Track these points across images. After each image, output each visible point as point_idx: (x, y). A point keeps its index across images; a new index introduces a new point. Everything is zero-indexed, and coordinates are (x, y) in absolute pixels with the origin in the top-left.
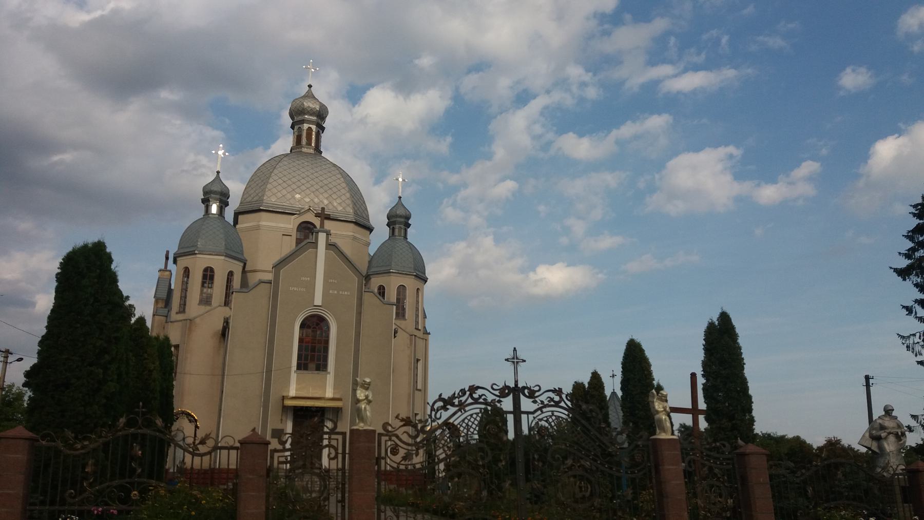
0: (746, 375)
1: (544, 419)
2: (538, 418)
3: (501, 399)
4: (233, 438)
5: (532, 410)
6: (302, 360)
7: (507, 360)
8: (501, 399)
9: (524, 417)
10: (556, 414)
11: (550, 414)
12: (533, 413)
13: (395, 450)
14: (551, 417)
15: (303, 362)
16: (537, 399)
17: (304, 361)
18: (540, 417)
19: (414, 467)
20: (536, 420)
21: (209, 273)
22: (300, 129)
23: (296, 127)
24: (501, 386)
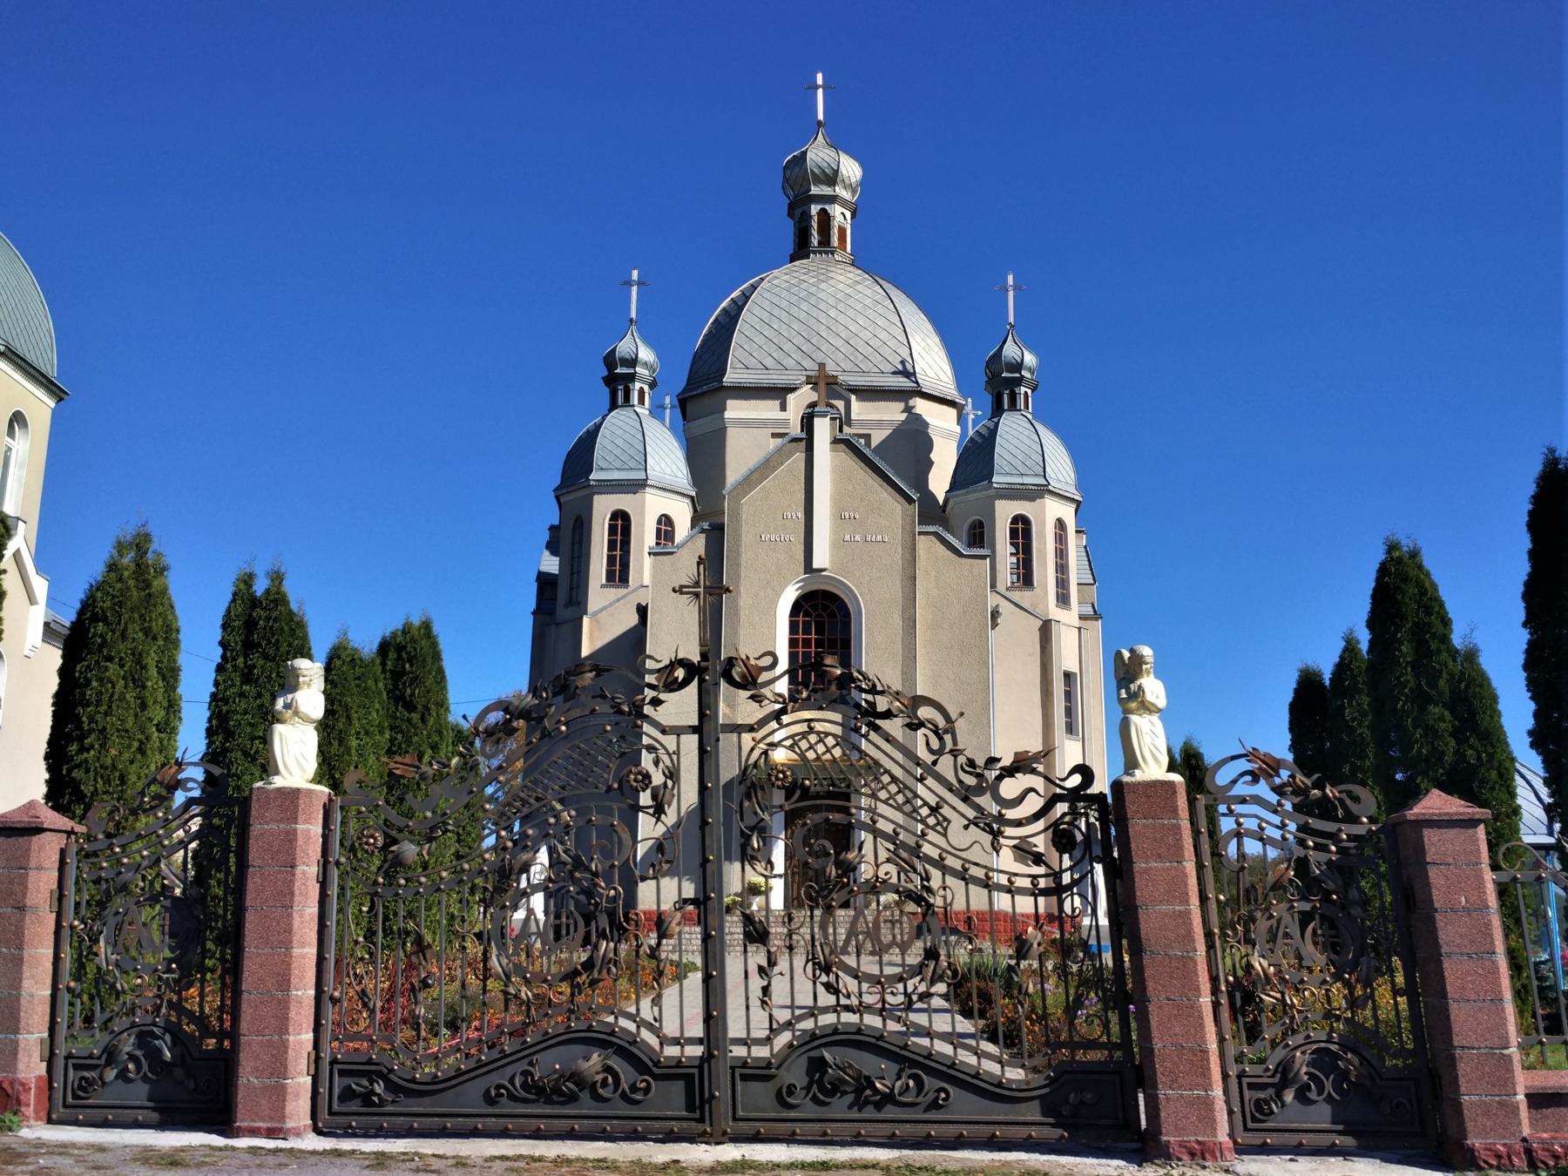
0: (1292, 695)
1: (784, 743)
2: (769, 740)
3: (662, 696)
4: (968, 849)
5: (751, 721)
6: (811, 639)
7: (679, 590)
8: (662, 696)
9: (727, 741)
10: (818, 727)
11: (803, 727)
12: (751, 729)
13: (1064, 841)
14: (804, 735)
15: (813, 636)
16: (766, 691)
17: (811, 639)
18: (777, 737)
19: (1032, 883)
20: (762, 746)
21: (1020, 526)
22: (806, 216)
23: (798, 212)
24: (666, 662)
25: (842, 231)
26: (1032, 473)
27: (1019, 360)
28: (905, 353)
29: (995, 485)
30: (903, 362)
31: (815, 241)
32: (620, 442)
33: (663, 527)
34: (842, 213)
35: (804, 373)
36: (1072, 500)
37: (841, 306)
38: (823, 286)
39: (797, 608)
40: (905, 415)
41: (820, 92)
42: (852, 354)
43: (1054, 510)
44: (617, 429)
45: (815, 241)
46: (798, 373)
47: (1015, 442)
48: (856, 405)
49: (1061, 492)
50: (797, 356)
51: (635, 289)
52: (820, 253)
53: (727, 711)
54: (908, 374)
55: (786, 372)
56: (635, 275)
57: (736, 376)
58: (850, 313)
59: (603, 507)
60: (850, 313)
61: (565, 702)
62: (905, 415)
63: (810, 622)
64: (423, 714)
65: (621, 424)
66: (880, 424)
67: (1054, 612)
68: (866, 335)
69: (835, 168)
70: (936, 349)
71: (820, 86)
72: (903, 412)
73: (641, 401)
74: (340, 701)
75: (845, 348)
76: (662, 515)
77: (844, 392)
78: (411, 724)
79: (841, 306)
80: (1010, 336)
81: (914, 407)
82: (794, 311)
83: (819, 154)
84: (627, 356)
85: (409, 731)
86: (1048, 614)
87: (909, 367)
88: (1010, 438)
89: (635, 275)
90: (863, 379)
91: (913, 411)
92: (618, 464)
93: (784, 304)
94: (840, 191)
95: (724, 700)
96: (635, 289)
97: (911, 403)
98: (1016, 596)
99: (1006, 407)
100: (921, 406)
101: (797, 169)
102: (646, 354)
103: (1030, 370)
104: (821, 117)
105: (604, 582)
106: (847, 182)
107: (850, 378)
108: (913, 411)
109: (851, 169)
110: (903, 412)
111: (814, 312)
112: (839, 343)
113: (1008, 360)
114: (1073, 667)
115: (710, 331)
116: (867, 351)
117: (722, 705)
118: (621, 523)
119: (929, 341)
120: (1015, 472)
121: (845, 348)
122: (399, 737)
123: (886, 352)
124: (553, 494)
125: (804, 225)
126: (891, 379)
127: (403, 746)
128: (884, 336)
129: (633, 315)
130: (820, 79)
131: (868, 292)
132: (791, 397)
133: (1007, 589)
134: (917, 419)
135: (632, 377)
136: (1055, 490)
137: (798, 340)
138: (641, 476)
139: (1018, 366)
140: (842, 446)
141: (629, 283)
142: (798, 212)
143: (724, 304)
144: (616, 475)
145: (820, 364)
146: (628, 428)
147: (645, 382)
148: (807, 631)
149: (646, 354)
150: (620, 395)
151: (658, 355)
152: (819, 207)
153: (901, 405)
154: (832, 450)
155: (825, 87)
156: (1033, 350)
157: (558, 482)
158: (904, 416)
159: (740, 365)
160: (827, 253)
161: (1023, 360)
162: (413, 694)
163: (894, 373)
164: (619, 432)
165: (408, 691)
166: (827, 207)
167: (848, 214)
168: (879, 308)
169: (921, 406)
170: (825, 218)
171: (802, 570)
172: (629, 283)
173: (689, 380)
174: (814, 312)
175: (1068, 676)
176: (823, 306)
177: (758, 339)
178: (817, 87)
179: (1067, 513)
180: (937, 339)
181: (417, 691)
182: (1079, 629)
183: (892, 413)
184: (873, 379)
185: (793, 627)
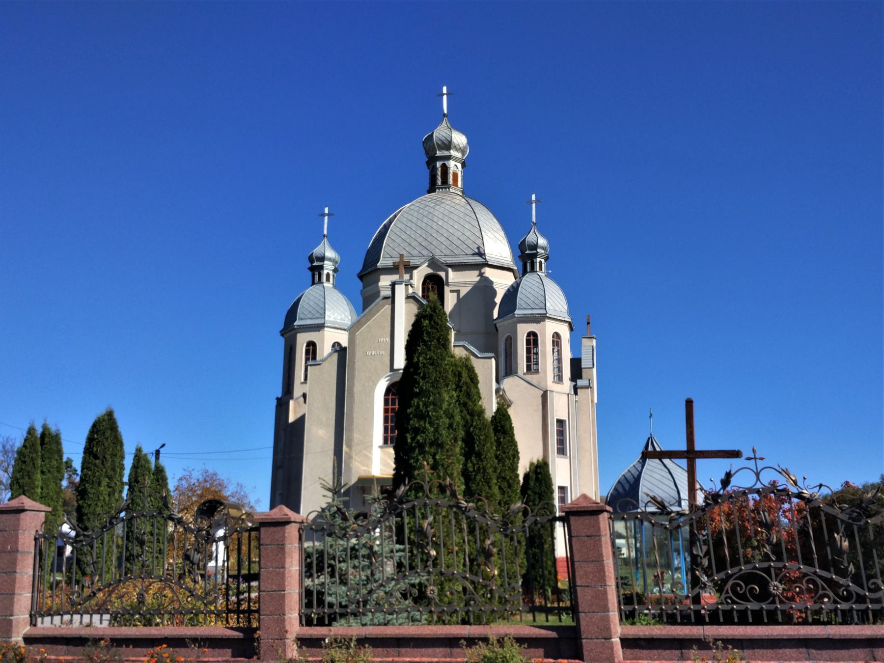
21: (532, 338)
23: (431, 166)
25: (455, 175)
26: (529, 307)
27: (536, 243)
28: (479, 242)
29: (516, 316)
30: (478, 248)
31: (439, 182)
32: (312, 303)
33: (555, 339)
34: (455, 165)
35: (423, 258)
36: (564, 321)
37: (446, 219)
38: (437, 208)
39: (388, 391)
40: (479, 278)
41: (445, 97)
42: (450, 245)
43: (549, 329)
44: (311, 294)
45: (439, 182)
46: (420, 258)
47: (530, 290)
48: (451, 273)
49: (555, 317)
50: (419, 248)
51: (326, 218)
52: (442, 188)
53: (347, 450)
54: (481, 254)
55: (413, 258)
56: (326, 210)
57: (385, 262)
58: (451, 222)
59: (302, 340)
60: (451, 222)
61: (139, 450)
62: (479, 278)
63: (395, 399)
64: (103, 461)
65: (314, 293)
66: (465, 284)
67: (550, 384)
68: (458, 234)
69: (450, 140)
70: (501, 239)
71: (445, 94)
72: (478, 276)
73: (541, 269)
74: (29, 456)
75: (446, 243)
76: (335, 343)
77: (445, 267)
78: (96, 466)
79: (446, 219)
80: (533, 230)
81: (484, 273)
82: (419, 223)
83: (441, 132)
84: (320, 256)
85: (94, 469)
86: (547, 387)
87: (481, 250)
88: (527, 288)
89: (326, 210)
90: (456, 259)
91: (484, 275)
92: (310, 316)
93: (414, 220)
94: (453, 153)
95: (346, 444)
96: (326, 218)
97: (483, 271)
98: (529, 377)
99: (528, 270)
100: (489, 272)
101: (429, 143)
102: (542, 241)
103: (543, 248)
104: (446, 112)
105: (525, 371)
106: (457, 147)
107: (448, 259)
108: (484, 275)
109: (459, 139)
110: (478, 276)
111: (430, 223)
112: (442, 239)
113: (529, 243)
114: (564, 417)
115: (376, 238)
116: (458, 243)
117: (344, 446)
118: (533, 340)
119: (496, 234)
120: (529, 307)
121: (446, 243)
122: (90, 473)
123: (469, 242)
124: (280, 334)
125: (434, 173)
126: (471, 258)
127: (91, 477)
128: (468, 234)
129: (325, 232)
130: (445, 90)
131: (462, 209)
132: (415, 272)
133: (524, 374)
134: (486, 280)
135: (535, 255)
136: (551, 316)
137: (420, 240)
138: (543, 312)
139: (535, 247)
140: (411, 300)
141: (323, 215)
142: (431, 166)
143: (385, 222)
144: (309, 322)
145: (400, 255)
146: (317, 295)
147: (330, 270)
148: (393, 403)
149: (542, 241)
150: (317, 277)
151: (549, 242)
152: (441, 163)
153: (477, 273)
154: (406, 303)
155: (448, 94)
156: (544, 235)
157: (282, 327)
158: (478, 279)
159: (388, 256)
160: (445, 188)
161: (537, 243)
162: (97, 451)
163: (473, 254)
164: (312, 298)
165: (95, 449)
166: (446, 162)
167: (459, 165)
168: (467, 219)
169: (489, 272)
170: (445, 169)
171: (389, 370)
172: (323, 215)
173: (364, 266)
174: (430, 223)
175: (560, 422)
176: (435, 219)
177: (398, 241)
178: (443, 94)
179: (564, 331)
180: (502, 233)
181: (99, 449)
182: (568, 394)
183: (472, 277)
184: (462, 259)
185: (386, 402)
